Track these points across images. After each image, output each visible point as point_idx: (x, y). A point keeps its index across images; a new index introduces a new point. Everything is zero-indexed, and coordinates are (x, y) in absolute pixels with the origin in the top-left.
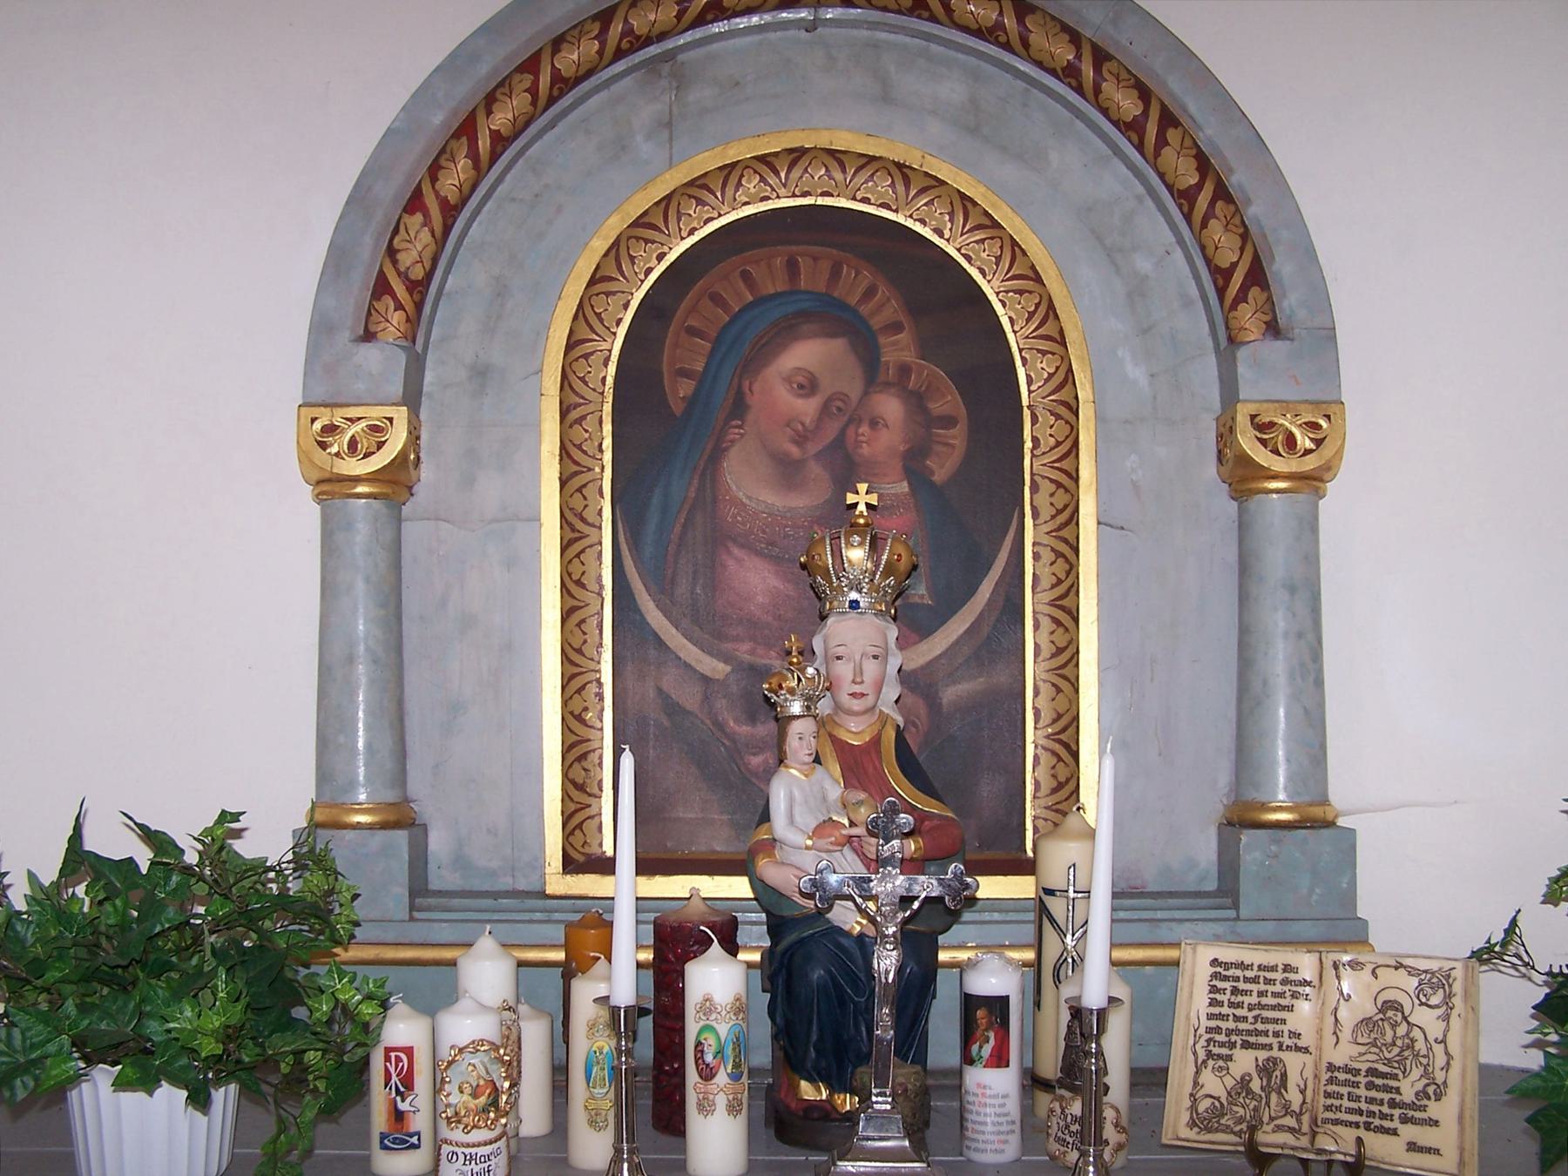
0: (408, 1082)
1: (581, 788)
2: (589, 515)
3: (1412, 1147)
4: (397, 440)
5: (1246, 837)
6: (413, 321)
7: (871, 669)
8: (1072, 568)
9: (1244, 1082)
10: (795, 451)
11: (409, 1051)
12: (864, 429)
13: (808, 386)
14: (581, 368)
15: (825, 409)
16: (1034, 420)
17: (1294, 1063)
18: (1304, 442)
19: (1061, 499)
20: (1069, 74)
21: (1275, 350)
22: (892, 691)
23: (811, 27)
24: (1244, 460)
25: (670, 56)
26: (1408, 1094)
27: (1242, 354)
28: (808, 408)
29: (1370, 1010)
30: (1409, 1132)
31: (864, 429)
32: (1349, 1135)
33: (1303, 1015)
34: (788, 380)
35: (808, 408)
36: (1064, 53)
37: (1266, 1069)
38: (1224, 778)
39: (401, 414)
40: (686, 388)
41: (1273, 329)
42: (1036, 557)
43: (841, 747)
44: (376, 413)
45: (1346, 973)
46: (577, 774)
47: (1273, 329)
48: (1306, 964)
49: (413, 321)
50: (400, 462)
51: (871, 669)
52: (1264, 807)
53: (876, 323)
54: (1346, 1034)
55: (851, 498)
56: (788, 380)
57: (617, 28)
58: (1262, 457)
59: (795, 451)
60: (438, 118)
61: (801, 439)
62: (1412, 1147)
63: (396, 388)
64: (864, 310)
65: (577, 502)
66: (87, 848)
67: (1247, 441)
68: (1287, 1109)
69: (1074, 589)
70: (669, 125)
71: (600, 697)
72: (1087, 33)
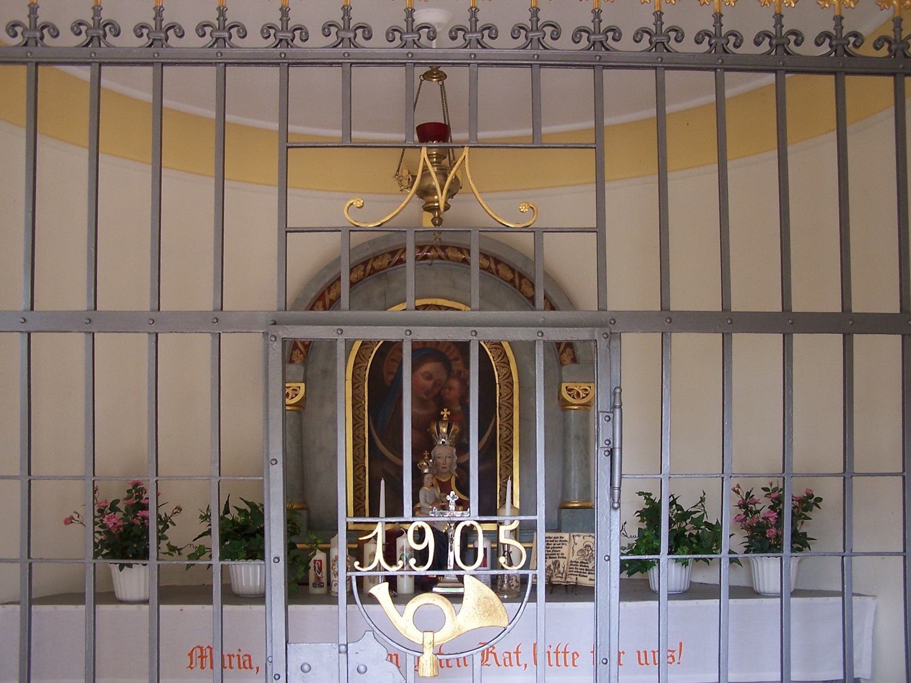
0: (320, 569)
1: (359, 498)
2: (361, 416)
3: (590, 579)
4: (302, 392)
5: (563, 511)
6: (306, 357)
7: (448, 460)
8: (511, 432)
9: (549, 567)
10: (425, 397)
11: (321, 561)
12: (447, 390)
13: (429, 377)
14: (358, 371)
15: (435, 385)
16: (500, 387)
17: (561, 561)
18: (582, 395)
19: (508, 411)
20: (512, 282)
21: (574, 367)
22: (455, 467)
23: (431, 265)
24: (564, 400)
25: (386, 273)
26: (590, 568)
27: (564, 368)
28: (429, 384)
29: (582, 547)
30: (590, 576)
31: (447, 390)
32: (575, 577)
33: (565, 550)
34: (422, 375)
35: (429, 384)
36: (510, 275)
37: (554, 564)
38: (559, 496)
39: (302, 385)
40: (391, 377)
41: (574, 360)
42: (500, 429)
43: (439, 482)
44: (294, 385)
45: (577, 538)
46: (358, 494)
47: (574, 360)
48: (566, 536)
49: (306, 357)
50: (304, 399)
51: (448, 460)
52: (570, 502)
53: (451, 358)
54: (575, 553)
55: (442, 413)
56: (422, 375)
57: (369, 267)
58: (569, 399)
59: (425, 397)
60: (313, 295)
61: (427, 393)
62: (590, 579)
63: (301, 378)
64: (447, 354)
65: (357, 412)
66: (854, 311)
67: (565, 394)
68: (559, 572)
69: (512, 439)
70: (385, 295)
71: (365, 471)
72: (517, 269)
